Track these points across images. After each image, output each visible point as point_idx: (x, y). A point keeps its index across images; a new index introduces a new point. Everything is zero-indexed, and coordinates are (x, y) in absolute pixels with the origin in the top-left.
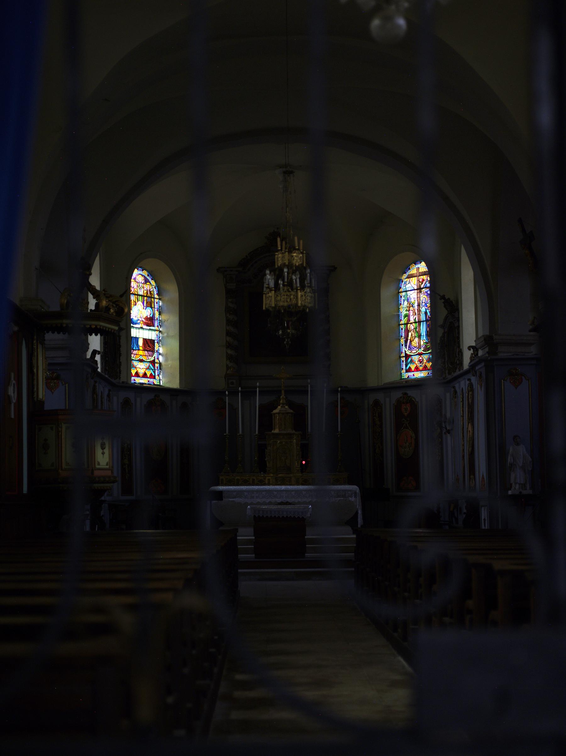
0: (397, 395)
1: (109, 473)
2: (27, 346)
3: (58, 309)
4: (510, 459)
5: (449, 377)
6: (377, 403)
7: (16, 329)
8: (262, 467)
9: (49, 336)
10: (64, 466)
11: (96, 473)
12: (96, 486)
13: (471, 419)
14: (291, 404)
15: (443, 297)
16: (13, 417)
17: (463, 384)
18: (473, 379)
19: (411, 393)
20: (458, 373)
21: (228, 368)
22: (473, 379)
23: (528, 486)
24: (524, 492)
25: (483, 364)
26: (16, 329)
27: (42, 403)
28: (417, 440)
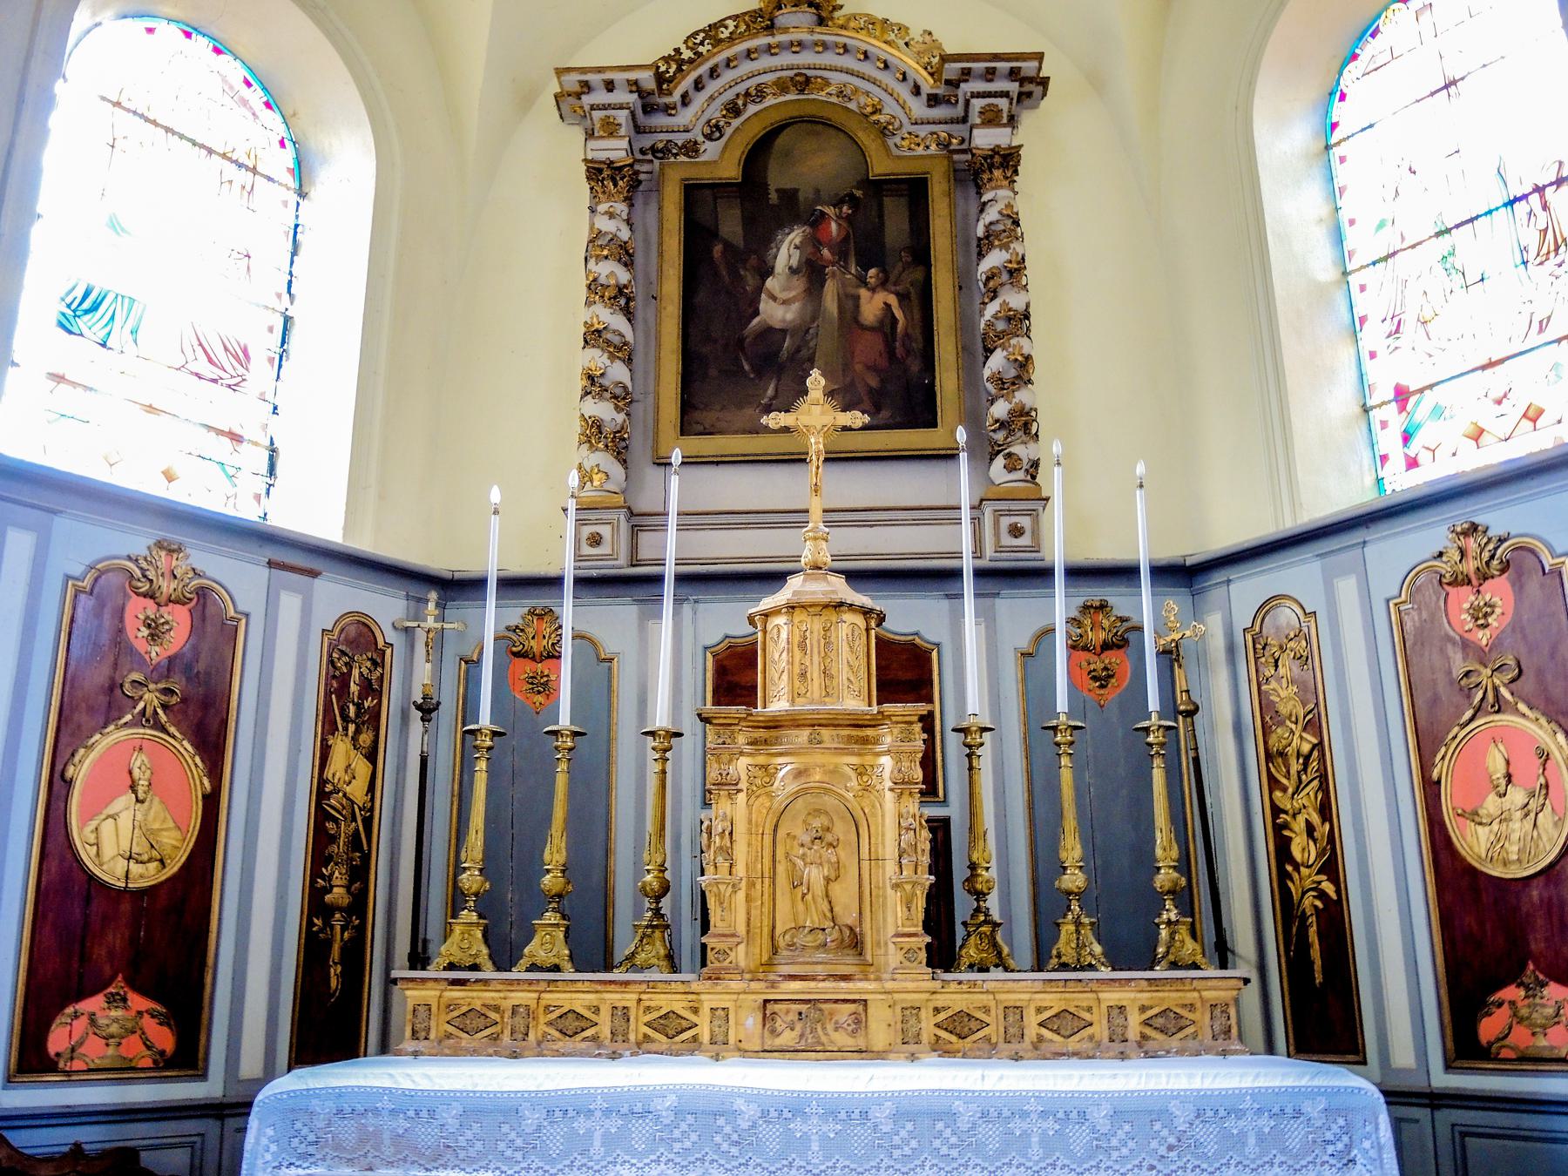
21: (586, 477)
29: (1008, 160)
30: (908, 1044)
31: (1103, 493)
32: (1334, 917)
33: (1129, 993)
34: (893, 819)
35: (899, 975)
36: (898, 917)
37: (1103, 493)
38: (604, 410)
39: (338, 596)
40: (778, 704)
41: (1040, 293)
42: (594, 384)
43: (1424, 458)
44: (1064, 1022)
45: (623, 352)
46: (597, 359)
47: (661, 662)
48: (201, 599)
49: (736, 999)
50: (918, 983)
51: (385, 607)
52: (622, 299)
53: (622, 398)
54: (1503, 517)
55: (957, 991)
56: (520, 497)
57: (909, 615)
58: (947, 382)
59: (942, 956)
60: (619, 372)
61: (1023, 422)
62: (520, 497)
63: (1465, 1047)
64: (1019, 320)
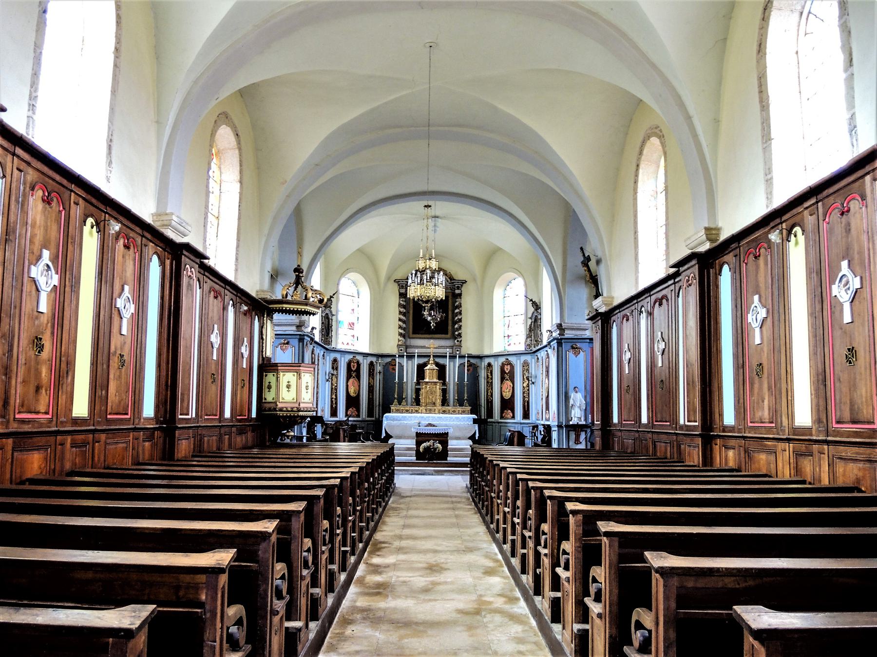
0: (502, 360)
1: (311, 405)
2: (259, 321)
3: (280, 298)
4: (571, 402)
5: (534, 349)
6: (489, 365)
7: (246, 308)
8: (417, 402)
9: (276, 316)
10: (281, 400)
11: (302, 405)
12: (301, 413)
13: (548, 375)
14: (437, 364)
15: (531, 300)
16: (245, 366)
17: (542, 354)
18: (550, 351)
19: (510, 358)
20: (540, 347)
21: (399, 341)
22: (550, 351)
23: (583, 419)
24: (580, 423)
25: (694, 262)
26: (246, 308)
27: (269, 359)
28: (513, 388)
29: (460, 295)
30: (439, 413)
31: (469, 346)
32: (336, 407)
33: (460, 409)
34: (439, 392)
35: (439, 406)
36: (439, 402)
37: (469, 346)
38: (402, 331)
39: (370, 359)
40: (427, 380)
41: (464, 316)
42: (400, 327)
43: (512, 344)
44: (454, 411)
45: (404, 322)
46: (401, 323)
47: (409, 369)
48: (358, 362)
49: (422, 408)
50: (440, 408)
51: (374, 359)
52: (404, 314)
53: (404, 329)
54: (510, 358)
55: (445, 408)
56: (391, 344)
57: (441, 361)
58: (450, 328)
59: (443, 405)
60: (404, 326)
61: (460, 335)
62: (391, 344)
63: (502, 417)
64: (460, 320)
